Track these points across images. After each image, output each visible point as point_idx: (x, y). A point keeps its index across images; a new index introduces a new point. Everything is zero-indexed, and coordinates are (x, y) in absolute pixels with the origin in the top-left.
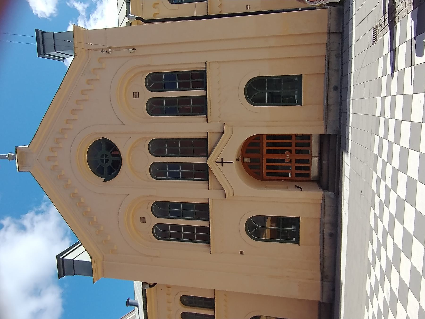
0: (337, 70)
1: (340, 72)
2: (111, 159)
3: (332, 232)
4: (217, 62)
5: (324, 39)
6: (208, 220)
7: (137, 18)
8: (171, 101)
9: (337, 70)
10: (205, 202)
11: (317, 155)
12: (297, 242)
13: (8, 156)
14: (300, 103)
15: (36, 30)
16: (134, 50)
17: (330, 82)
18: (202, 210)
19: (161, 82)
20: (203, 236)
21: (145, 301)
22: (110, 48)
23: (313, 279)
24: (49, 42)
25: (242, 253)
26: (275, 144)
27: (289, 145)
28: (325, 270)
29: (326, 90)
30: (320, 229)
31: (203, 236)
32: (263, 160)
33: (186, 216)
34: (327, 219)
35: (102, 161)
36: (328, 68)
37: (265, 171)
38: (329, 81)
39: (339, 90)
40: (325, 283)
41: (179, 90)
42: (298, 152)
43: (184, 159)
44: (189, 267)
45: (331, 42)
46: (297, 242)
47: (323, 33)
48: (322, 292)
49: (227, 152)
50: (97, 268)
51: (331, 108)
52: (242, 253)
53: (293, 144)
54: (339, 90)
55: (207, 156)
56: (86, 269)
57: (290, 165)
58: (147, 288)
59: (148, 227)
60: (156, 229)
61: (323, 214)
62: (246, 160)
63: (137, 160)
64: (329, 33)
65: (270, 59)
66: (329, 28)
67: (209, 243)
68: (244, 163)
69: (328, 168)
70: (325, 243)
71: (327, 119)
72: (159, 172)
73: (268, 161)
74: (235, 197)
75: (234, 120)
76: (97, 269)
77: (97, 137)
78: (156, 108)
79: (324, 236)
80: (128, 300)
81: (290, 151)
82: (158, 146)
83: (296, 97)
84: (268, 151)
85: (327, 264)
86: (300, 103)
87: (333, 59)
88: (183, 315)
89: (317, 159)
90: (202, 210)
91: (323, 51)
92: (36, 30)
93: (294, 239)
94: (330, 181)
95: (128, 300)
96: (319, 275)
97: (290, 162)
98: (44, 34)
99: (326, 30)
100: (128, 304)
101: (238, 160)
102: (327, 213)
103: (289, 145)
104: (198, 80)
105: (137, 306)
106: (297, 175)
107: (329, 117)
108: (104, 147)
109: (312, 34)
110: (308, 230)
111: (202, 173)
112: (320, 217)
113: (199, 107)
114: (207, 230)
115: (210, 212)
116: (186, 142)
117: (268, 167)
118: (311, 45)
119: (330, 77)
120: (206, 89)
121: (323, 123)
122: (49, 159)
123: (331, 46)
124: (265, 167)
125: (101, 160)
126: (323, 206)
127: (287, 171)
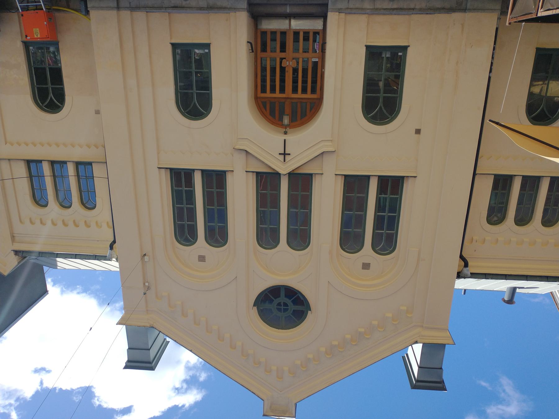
2: (283, 299)
4: (158, 153)
5: (126, 14)
6: (368, 177)
8: (209, 216)
11: (287, 21)
12: (405, 49)
14: (207, 46)
15: (126, 367)
16: (145, 255)
18: (354, 185)
20: (392, 186)
22: (144, 284)
23: (463, 25)
24: (139, 355)
26: (283, 81)
28: (447, 5)
29: (225, 11)
31: (392, 186)
32: (295, 98)
33: (363, 206)
37: (309, 95)
40: (469, 6)
41: (195, 205)
43: (283, 205)
44: (435, 209)
45: (128, 6)
46: (405, 49)
48: (483, 10)
49: (269, 146)
50: (433, 336)
52: (418, 132)
55: (276, 175)
56: (433, 351)
58: (468, 270)
60: (381, 250)
62: (286, 121)
63: (283, 266)
64: (118, 8)
66: (111, 8)
67: (403, 178)
68: (290, 126)
70: (405, 7)
72: (300, 237)
73: (295, 90)
74: (339, 139)
75: (234, 134)
76: (437, 338)
78: (218, 235)
80: (504, 301)
81: (282, 59)
82: (267, 236)
83: (201, 52)
84: (282, 90)
86: (207, 46)
88: (547, 222)
90: (354, 185)
91: (140, 15)
93: (400, 54)
95: (504, 301)
96: (457, 16)
98: (131, 359)
99: (115, 12)
100: (510, 301)
101: (286, 133)
102: (358, 6)
105: (514, 289)
108: (267, 305)
111: (302, 182)
112: (367, 15)
113: (216, 180)
114: (383, 181)
116: (347, 204)
117: (304, 91)
118: (133, 32)
119: (173, 5)
120: (193, 170)
121: (232, 14)
124: (304, 96)
125: (284, 312)
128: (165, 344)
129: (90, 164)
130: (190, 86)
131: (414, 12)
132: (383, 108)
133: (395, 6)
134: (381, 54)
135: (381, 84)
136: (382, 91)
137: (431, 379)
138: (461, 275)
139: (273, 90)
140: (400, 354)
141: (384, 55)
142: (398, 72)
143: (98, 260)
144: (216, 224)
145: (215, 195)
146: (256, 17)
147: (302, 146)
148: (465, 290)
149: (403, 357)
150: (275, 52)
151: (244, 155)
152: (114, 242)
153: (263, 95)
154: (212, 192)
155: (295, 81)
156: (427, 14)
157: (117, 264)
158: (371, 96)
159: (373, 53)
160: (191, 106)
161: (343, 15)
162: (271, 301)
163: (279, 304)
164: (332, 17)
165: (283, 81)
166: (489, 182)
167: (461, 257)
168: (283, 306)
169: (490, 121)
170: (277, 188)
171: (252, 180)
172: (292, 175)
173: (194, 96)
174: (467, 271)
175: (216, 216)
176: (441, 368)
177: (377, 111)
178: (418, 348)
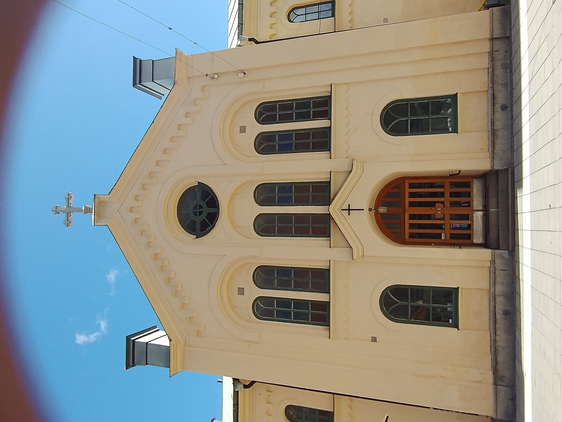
0: (505, 85)
1: (509, 86)
2: (206, 210)
3: (508, 308)
5: (486, 47)
7: (250, 40)
8: (285, 135)
9: (505, 85)
10: (324, 266)
11: (481, 208)
12: (456, 325)
13: (84, 209)
14: (455, 131)
15: (134, 57)
17: (495, 100)
19: (273, 225)
20: (320, 315)
21: (236, 410)
22: (216, 74)
23: (481, 382)
25: (374, 340)
26: (421, 204)
27: (442, 195)
28: (499, 367)
30: (490, 304)
31: (320, 315)
33: (299, 287)
34: (499, 289)
35: (195, 213)
36: (493, 82)
37: (407, 231)
38: (494, 99)
39: (509, 109)
40: (500, 388)
41: (294, 123)
42: (453, 204)
44: (299, 359)
45: (494, 50)
46: (456, 325)
47: (484, 39)
48: (496, 402)
51: (500, 133)
52: (374, 340)
53: (447, 194)
54: (509, 109)
55: (328, 202)
56: (164, 356)
57: (442, 222)
58: (241, 388)
59: (247, 301)
61: (494, 283)
62: (382, 210)
63: (239, 210)
64: (492, 39)
65: (414, 77)
67: (329, 325)
69: (498, 219)
70: (497, 326)
71: (493, 147)
72: (266, 227)
73: (412, 217)
74: (365, 262)
75: (367, 158)
77: (193, 183)
78: (266, 145)
79: (495, 314)
81: (443, 203)
82: (267, 193)
84: (412, 204)
85: (501, 357)
86: (455, 131)
87: (499, 71)
89: (480, 213)
90: (319, 279)
91: (485, 62)
92: (134, 57)
93: (451, 321)
94: (502, 237)
97: (443, 219)
99: (488, 36)
101: (370, 210)
102: (498, 279)
103: (442, 195)
104: (320, 140)
106: (453, 236)
107: (496, 146)
108: (199, 196)
109: (468, 41)
110: (473, 307)
111: (321, 227)
114: (325, 307)
115: (331, 188)
117: (412, 226)
119: (496, 95)
120: (330, 119)
121: (488, 155)
122: (131, 210)
123: (496, 54)
124: (407, 226)
126: (493, 271)
127: (438, 231)
128: (158, 95)
129: (333, 15)
130: (414, 114)
131: (492, 335)
132: (397, 305)
133: (498, 316)
134: (451, 302)
135: (420, 303)
136: (414, 304)
137: (135, 354)
138: (236, 382)
139: (412, 195)
140: (159, 325)
141: (449, 305)
142: (433, 318)
143: (238, 26)
144: (277, 143)
145: (307, 141)
146: (484, 176)
147: (357, 224)
148: (221, 382)
149: (155, 327)
150: (451, 197)
151: (348, 169)
152: (257, 42)
153: (407, 185)
154: (309, 138)
155: (420, 217)
156: (491, 347)
157: (234, 46)
158: (408, 294)
159: (449, 295)
160: (394, 115)
161: (488, 264)
162: (203, 199)
163: (201, 207)
164: (486, 254)
165: (421, 204)
166: (327, 408)
167: (253, 383)
168: (199, 211)
169: (388, 417)
170: (316, 202)
171: (323, 178)
172: (327, 218)
173: (404, 118)
174: (240, 388)
175: (285, 142)
176: (147, 364)
177: (393, 299)
178: (165, 342)
